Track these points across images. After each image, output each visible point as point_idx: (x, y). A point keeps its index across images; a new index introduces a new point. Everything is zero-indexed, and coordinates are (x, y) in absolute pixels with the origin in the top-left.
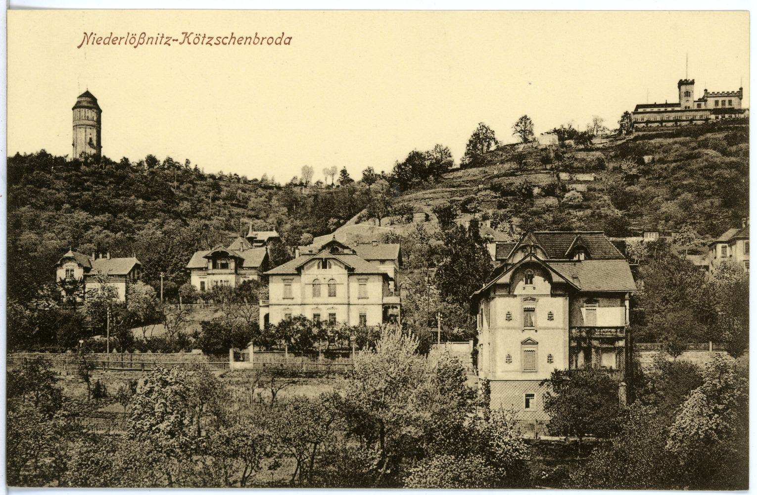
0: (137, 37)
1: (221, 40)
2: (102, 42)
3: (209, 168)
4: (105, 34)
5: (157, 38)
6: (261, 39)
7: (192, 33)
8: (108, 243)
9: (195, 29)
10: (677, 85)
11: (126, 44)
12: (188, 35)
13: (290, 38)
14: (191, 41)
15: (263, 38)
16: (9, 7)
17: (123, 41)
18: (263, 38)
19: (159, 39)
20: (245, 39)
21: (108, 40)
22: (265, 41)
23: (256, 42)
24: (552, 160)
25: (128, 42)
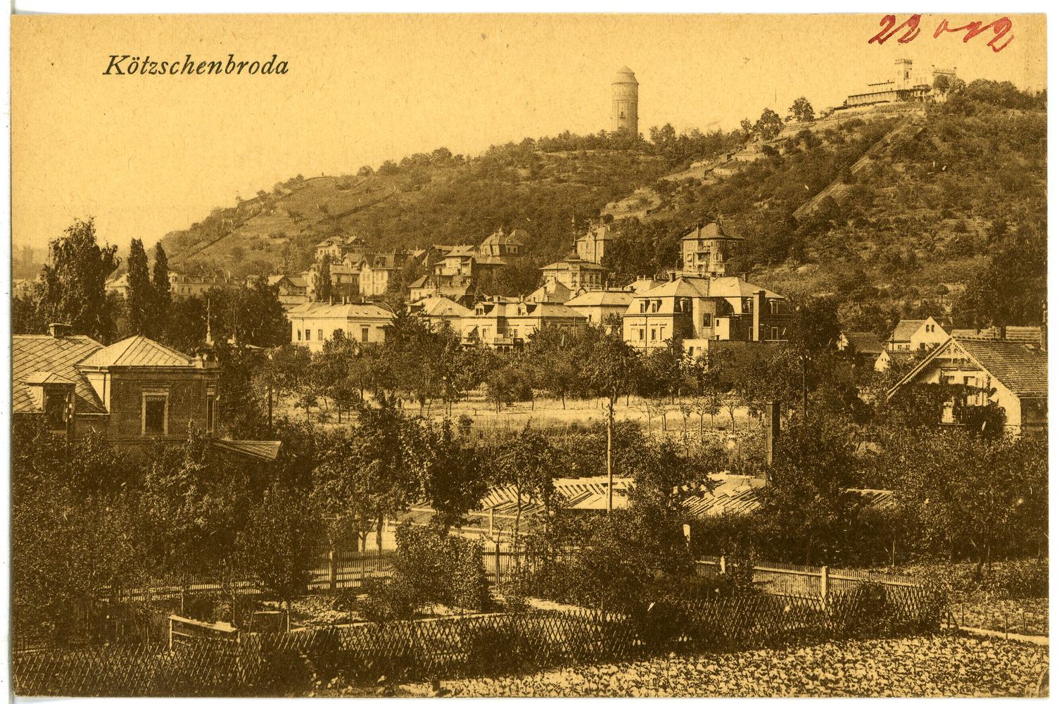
7: (125, 57)
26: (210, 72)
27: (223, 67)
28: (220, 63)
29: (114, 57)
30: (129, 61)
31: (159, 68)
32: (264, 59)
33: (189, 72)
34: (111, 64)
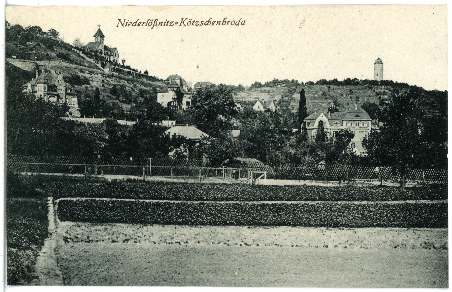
0: (153, 22)
1: (204, 23)
2: (131, 25)
3: (428, 87)
4: (206, 20)
6: (227, 22)
7: (186, 19)
8: (20, 178)
9: (189, 16)
10: (319, 80)
11: (117, 26)
12: (183, 20)
13: (245, 21)
15: (228, 22)
16: (7, 5)
17: (145, 24)
18: (228, 22)
19: (166, 23)
20: (142, 23)
21: (238, 22)
22: (229, 23)
24: (311, 147)
25: (147, 25)
26: (159, 25)
28: (220, 22)
29: (182, 19)
30: (188, 20)
31: (200, 23)
32: (133, 21)
33: (161, 25)
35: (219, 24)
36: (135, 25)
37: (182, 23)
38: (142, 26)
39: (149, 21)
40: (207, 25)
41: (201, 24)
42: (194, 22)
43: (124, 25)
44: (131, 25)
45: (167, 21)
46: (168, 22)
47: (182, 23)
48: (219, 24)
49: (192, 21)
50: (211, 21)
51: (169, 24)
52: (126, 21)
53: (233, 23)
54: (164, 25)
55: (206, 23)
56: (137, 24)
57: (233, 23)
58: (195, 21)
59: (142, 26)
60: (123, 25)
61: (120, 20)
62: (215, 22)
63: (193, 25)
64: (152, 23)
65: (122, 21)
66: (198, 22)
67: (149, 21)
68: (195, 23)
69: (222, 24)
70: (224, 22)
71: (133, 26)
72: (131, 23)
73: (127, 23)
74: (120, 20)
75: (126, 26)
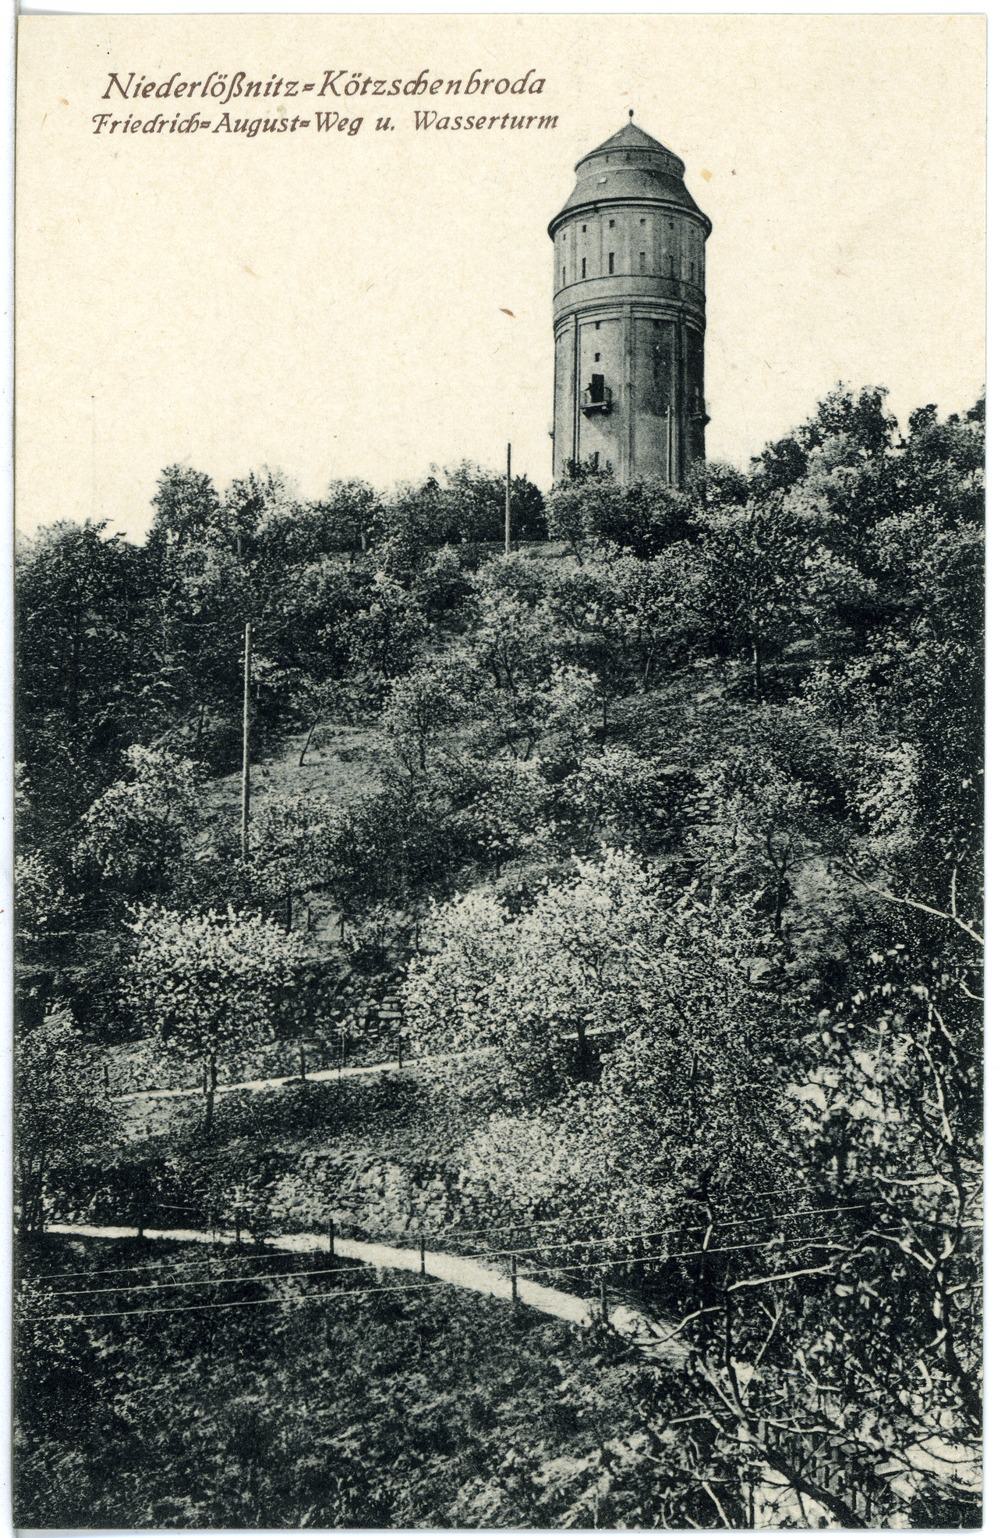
2: (153, 93)
5: (269, 84)
7: (342, 73)
14: (340, 88)
17: (199, 90)
18: (487, 83)
20: (189, 88)
21: (165, 88)
23: (217, 91)
25: (208, 91)
27: (262, 89)
28: (459, 82)
29: (329, 73)
30: (347, 78)
31: (388, 87)
32: (409, 76)
33: (256, 94)
34: (325, 85)
35: (456, 92)
36: (521, 91)
37: (329, 87)
38: (190, 95)
39: (215, 79)
40: (414, 92)
41: (394, 91)
42: (368, 81)
43: (130, 93)
44: (153, 93)
45: (277, 80)
46: (279, 84)
47: (329, 87)
48: (456, 92)
49: (361, 81)
50: (426, 82)
51: (283, 89)
52: (136, 80)
53: (502, 86)
54: (266, 94)
55: (411, 87)
56: (140, 92)
57: (502, 86)
58: (374, 80)
59: (190, 95)
60: (124, 94)
61: (114, 76)
62: (441, 82)
63: (364, 92)
64: (357, 84)
65: (123, 80)
66: (383, 83)
67: (215, 79)
68: (370, 88)
69: (467, 92)
70: (474, 85)
71: (158, 95)
72: (153, 85)
73: (139, 86)
74: (114, 76)
75: (135, 95)
